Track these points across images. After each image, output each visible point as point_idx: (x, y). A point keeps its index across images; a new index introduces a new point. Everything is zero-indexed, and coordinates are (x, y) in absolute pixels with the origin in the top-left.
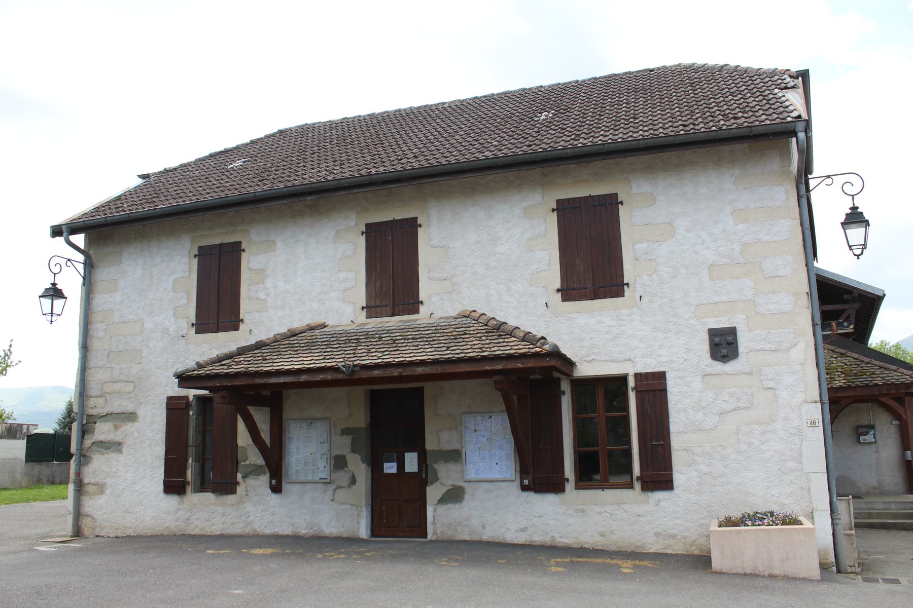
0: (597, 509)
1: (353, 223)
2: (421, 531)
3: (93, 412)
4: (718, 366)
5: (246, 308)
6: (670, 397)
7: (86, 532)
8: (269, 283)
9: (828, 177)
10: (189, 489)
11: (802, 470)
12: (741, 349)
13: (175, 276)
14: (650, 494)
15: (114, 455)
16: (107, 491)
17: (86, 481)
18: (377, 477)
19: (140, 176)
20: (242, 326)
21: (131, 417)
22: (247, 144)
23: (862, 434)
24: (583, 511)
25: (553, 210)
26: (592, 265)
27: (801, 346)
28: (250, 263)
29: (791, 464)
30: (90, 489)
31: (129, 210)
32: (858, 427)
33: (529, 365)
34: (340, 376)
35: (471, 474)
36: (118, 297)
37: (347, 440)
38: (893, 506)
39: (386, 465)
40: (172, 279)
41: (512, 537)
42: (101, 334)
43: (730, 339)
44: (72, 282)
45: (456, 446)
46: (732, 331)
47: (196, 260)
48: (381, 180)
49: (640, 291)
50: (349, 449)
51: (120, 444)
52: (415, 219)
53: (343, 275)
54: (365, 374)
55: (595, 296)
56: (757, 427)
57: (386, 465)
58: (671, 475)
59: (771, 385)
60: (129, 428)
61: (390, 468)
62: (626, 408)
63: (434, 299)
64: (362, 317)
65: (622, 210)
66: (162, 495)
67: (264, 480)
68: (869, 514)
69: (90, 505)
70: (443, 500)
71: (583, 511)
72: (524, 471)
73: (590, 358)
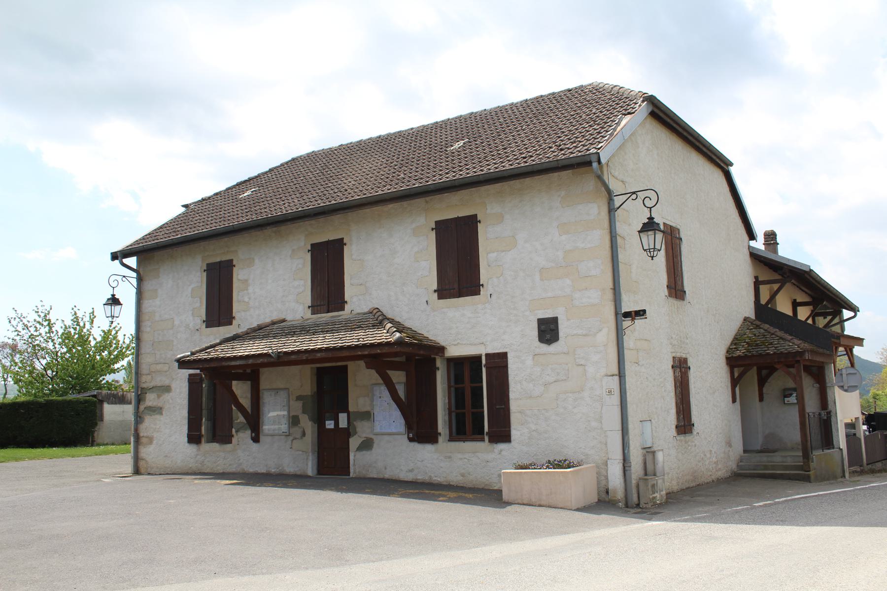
0: (460, 456)
1: (302, 244)
2: (344, 469)
3: (144, 386)
4: (544, 348)
5: (349, 292)
6: (509, 370)
7: (142, 470)
8: (251, 290)
9: (634, 193)
10: (203, 440)
11: (602, 428)
12: (561, 334)
13: (193, 286)
14: (495, 445)
15: (158, 416)
16: (154, 442)
17: (141, 435)
18: (321, 431)
19: (183, 206)
20: (234, 322)
21: (167, 389)
22: (266, 173)
23: (785, 396)
24: (450, 457)
25: (433, 229)
26: (459, 272)
27: (605, 331)
28: (239, 275)
29: (594, 424)
30: (144, 440)
31: (162, 239)
32: (785, 390)
33: (384, 351)
34: (272, 360)
35: (377, 429)
36: (157, 302)
37: (299, 404)
38: (789, 459)
39: (327, 422)
40: (190, 289)
41: (404, 475)
42: (148, 329)
43: (552, 327)
44: (128, 293)
45: (368, 409)
46: (555, 320)
47: (205, 274)
48: (311, 208)
49: (491, 291)
50: (301, 411)
51: (161, 408)
52: (232, 260)
53: (296, 283)
54: (286, 359)
55: (460, 295)
56: (570, 395)
57: (327, 422)
58: (510, 431)
59: (582, 362)
60: (166, 397)
61: (330, 424)
62: (482, 382)
63: (355, 299)
64: (308, 314)
65: (480, 227)
66: (187, 444)
67: (247, 434)
68: (765, 466)
69: (144, 452)
70: (361, 448)
71: (450, 457)
72: (409, 426)
73: (456, 343)
